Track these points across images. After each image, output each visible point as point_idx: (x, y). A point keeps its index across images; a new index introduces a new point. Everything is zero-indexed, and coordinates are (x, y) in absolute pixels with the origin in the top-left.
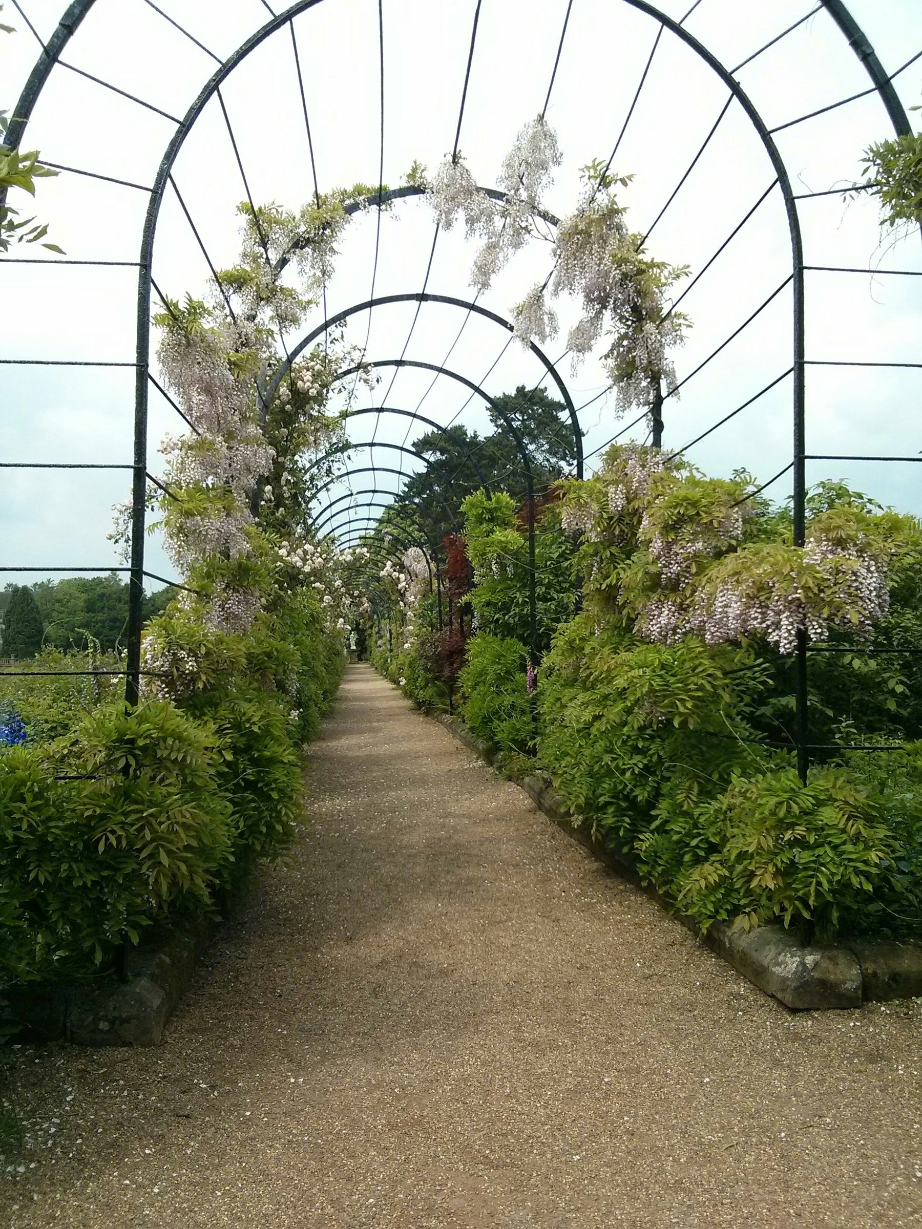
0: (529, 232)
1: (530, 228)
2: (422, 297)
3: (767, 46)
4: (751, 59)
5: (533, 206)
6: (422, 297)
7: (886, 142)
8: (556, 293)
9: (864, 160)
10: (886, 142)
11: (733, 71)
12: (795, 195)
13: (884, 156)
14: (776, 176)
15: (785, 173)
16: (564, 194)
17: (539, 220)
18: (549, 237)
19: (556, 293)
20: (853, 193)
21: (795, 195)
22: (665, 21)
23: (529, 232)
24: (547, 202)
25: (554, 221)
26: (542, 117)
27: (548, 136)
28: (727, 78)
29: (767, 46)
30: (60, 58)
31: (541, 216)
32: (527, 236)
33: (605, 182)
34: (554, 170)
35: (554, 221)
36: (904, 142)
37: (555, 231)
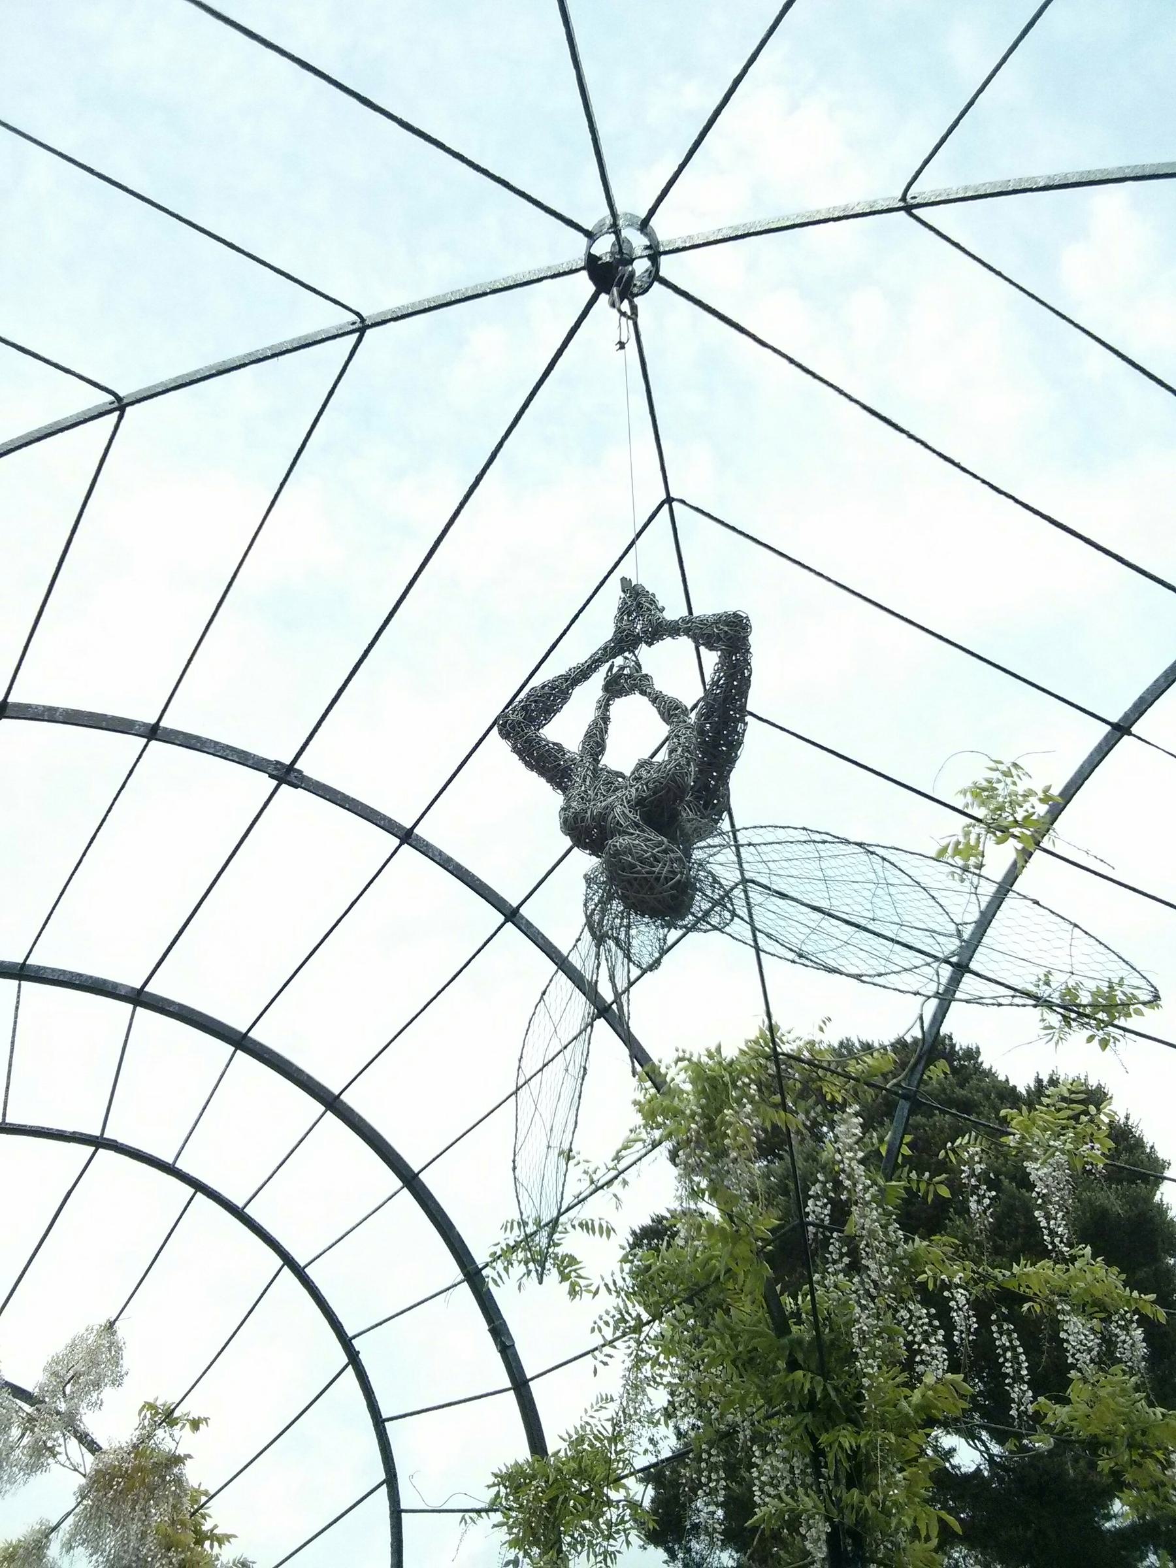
0: (55, 1456)
1: (57, 1449)
2: (99, 1142)
3: (398, 1315)
4: (377, 1325)
5: (71, 1424)
6: (99, 1142)
7: (517, 1463)
8: (69, 1547)
9: (494, 1485)
10: (517, 1463)
11: (355, 1337)
12: (100, 1150)
13: (514, 1480)
14: (383, 1477)
15: (395, 1475)
16: (114, 1422)
17: (73, 1443)
18: (81, 1470)
19: (69, 1547)
20: (474, 1515)
21: (403, 1507)
22: (288, 1260)
23: (55, 1456)
24: (90, 1422)
25: (93, 1447)
26: (112, 1324)
27: (115, 1350)
28: (346, 1342)
29: (398, 1315)
30: (416, 1171)
31: (76, 1437)
32: (50, 1460)
33: (168, 1417)
34: (108, 1393)
35: (93, 1447)
36: (536, 1465)
37: (89, 1461)
